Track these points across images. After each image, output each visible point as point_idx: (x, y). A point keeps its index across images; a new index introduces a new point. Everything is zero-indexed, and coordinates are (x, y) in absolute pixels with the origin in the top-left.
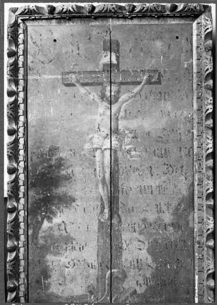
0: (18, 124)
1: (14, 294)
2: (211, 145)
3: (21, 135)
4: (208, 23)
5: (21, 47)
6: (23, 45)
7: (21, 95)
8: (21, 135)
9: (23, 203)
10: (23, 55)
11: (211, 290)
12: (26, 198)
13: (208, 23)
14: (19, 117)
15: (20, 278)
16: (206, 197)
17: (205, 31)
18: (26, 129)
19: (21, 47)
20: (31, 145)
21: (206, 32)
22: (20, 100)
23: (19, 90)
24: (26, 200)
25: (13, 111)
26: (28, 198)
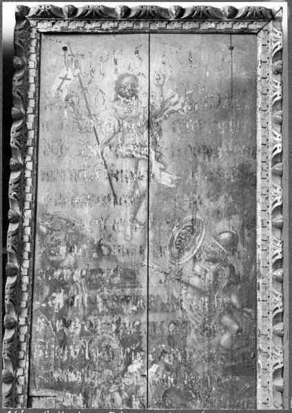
0: (25, 158)
1: (12, 332)
2: (278, 93)
3: (27, 222)
4: (276, 36)
5: (26, 264)
6: (29, 228)
7: (31, 118)
8: (27, 222)
9: (31, 169)
10: (34, 113)
11: (279, 391)
12: (36, 130)
13: (276, 36)
14: (29, 101)
15: (25, 251)
16: (273, 374)
17: (273, 204)
18: (35, 180)
19: (26, 264)
20: (40, 210)
21: (274, 101)
22: (30, 125)
23: (28, 112)
24: (32, 263)
25: (17, 192)
26: (34, 259)
